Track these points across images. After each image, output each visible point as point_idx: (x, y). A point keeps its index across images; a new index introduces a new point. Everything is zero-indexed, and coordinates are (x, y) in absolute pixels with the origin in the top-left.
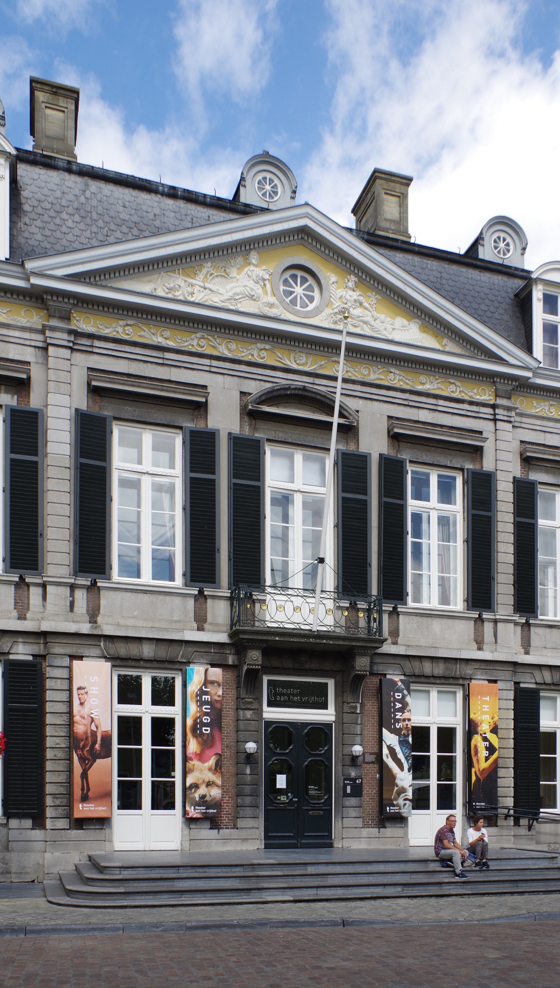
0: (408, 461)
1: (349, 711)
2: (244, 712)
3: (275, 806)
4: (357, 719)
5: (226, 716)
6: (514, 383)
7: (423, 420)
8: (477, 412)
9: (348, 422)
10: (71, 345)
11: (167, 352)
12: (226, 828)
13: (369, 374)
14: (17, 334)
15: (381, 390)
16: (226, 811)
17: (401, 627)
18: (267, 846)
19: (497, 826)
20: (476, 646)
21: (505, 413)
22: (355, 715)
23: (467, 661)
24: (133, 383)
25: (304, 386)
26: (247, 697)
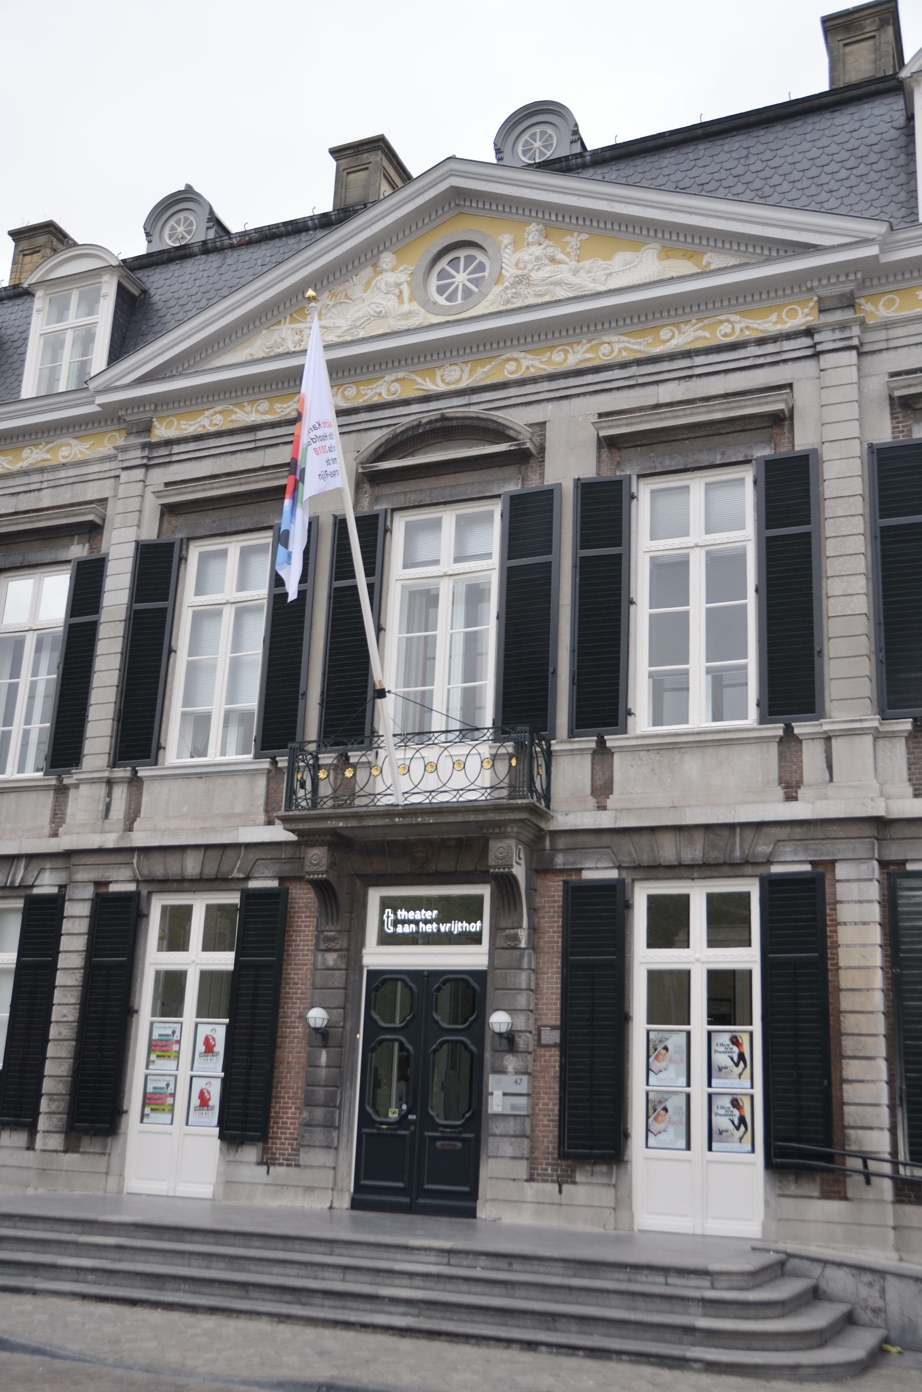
0: (634, 478)
1: (505, 945)
2: (323, 956)
3: (441, 1132)
4: (521, 960)
5: (303, 965)
6: (852, 277)
7: (668, 400)
8: (778, 353)
9: (515, 445)
10: (145, 461)
11: (261, 430)
12: (289, 1165)
13: (565, 360)
14: (96, 468)
15: (585, 377)
16: (290, 1134)
17: (617, 776)
18: (356, 1205)
19: (845, 1198)
20: (780, 792)
21: (838, 335)
22: (518, 952)
23: (760, 826)
24: (204, 487)
25: (442, 414)
26: (327, 928)
